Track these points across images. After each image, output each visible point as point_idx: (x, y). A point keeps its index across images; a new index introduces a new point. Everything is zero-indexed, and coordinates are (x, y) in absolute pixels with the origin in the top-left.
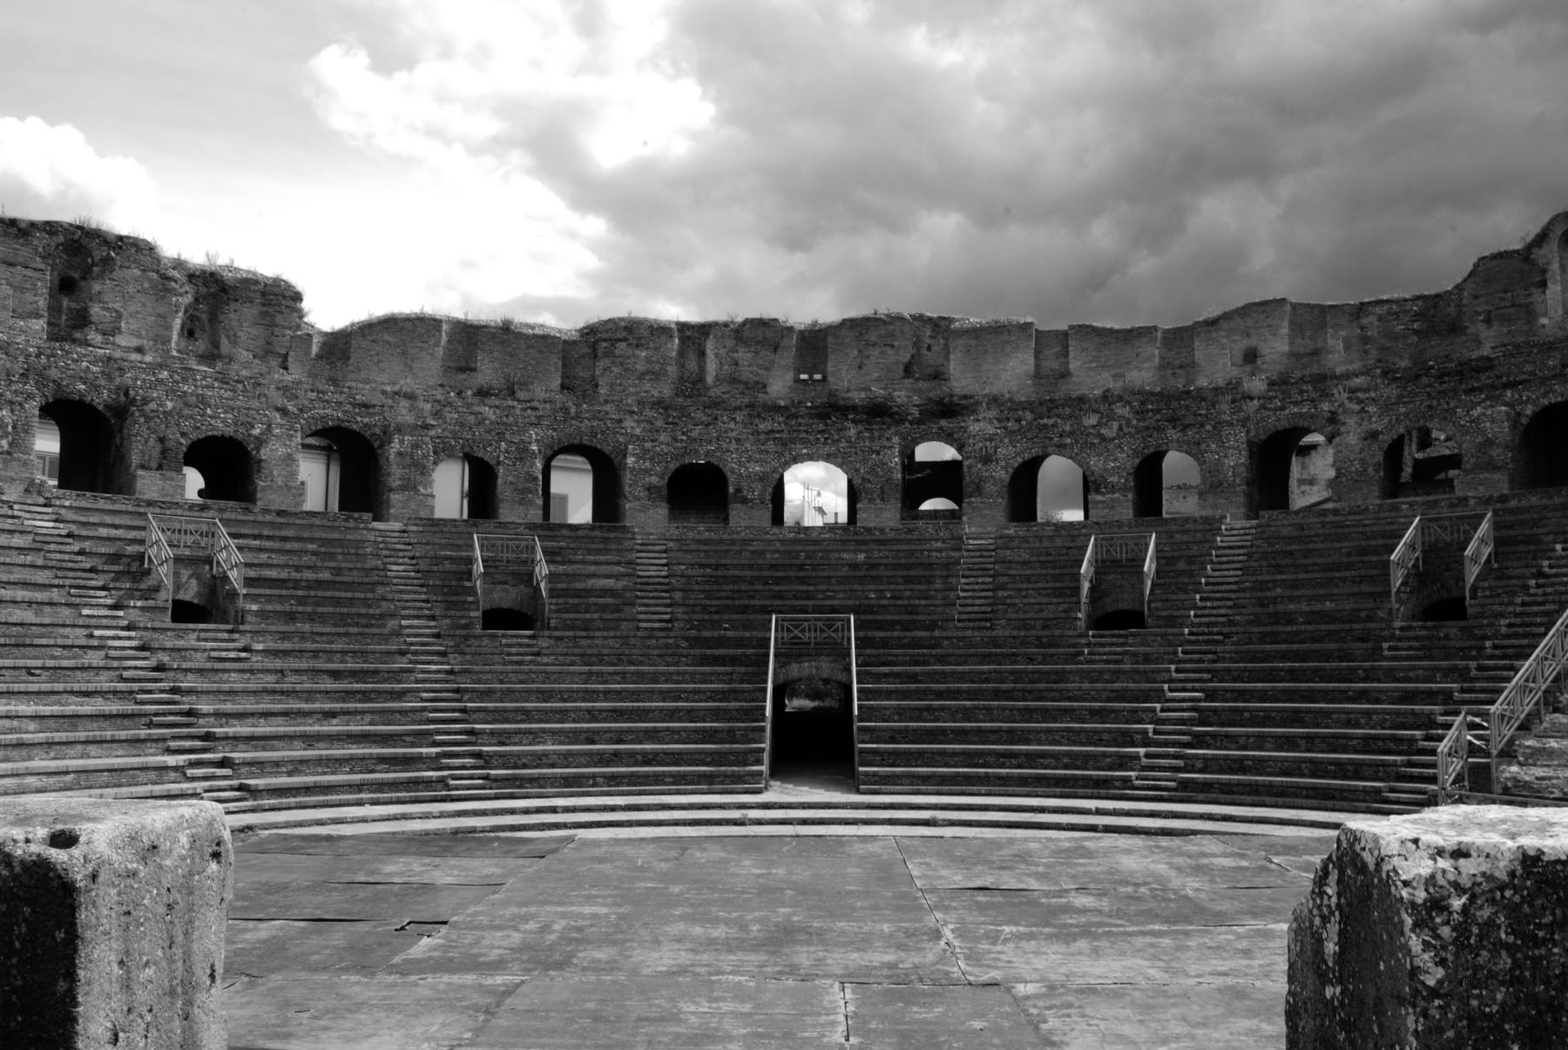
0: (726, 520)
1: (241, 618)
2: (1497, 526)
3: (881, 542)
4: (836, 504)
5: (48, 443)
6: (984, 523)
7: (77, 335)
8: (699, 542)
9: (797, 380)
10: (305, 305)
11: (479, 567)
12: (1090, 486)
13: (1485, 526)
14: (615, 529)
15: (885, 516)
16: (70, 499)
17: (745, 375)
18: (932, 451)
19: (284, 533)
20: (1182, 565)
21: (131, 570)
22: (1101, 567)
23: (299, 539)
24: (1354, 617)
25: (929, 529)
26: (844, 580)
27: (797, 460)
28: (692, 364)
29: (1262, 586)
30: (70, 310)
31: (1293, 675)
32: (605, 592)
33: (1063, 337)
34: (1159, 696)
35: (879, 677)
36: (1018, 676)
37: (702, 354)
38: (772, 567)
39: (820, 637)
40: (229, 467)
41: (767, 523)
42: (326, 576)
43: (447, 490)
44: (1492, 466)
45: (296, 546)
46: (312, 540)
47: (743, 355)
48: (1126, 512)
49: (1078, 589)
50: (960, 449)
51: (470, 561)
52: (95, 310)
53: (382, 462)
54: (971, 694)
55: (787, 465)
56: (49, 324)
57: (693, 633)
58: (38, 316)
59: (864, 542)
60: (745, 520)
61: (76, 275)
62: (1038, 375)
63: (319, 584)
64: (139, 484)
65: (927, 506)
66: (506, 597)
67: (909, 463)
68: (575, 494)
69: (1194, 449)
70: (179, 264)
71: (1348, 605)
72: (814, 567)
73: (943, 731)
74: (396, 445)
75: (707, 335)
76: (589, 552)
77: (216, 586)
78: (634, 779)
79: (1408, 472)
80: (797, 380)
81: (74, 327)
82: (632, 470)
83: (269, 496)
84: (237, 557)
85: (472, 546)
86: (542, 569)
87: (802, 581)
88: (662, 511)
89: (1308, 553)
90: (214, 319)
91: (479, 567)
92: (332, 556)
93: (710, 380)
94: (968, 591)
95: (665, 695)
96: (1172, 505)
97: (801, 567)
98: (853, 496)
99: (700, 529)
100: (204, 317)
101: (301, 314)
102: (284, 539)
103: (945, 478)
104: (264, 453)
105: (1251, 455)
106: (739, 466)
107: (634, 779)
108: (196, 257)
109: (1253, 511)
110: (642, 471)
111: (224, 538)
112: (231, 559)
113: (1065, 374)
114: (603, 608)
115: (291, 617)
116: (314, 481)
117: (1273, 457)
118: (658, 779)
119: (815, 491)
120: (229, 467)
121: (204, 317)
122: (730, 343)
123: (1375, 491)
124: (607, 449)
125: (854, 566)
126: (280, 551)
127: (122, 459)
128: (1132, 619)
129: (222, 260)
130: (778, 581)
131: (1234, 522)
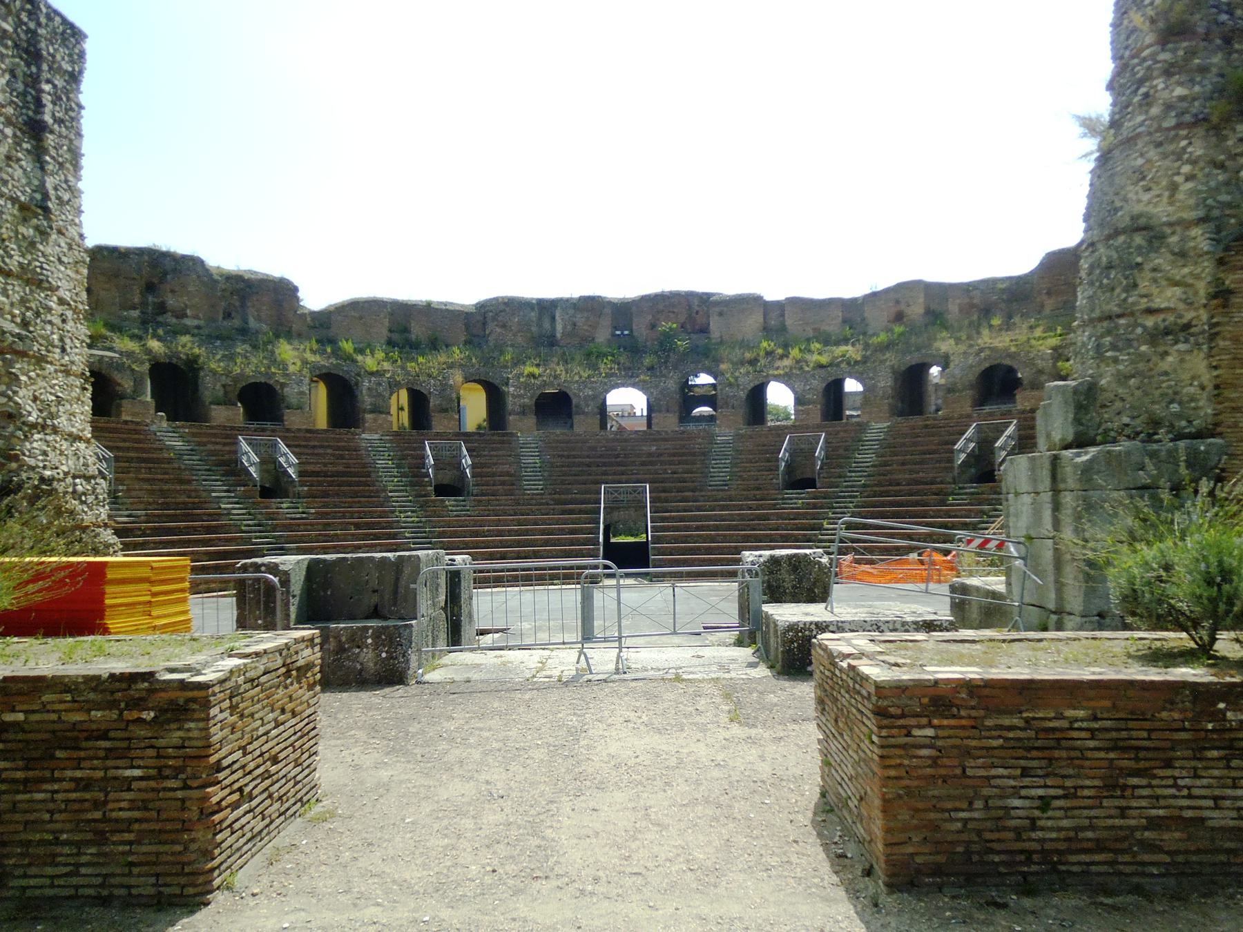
0: (572, 426)
2: (1019, 428)
3: (665, 440)
7: (160, 319)
8: (558, 441)
9: (614, 335)
10: (300, 294)
13: (1011, 429)
14: (504, 435)
15: (669, 422)
19: (312, 443)
20: (841, 451)
22: (793, 452)
23: (321, 447)
30: (154, 303)
34: (820, 528)
35: (663, 519)
36: (742, 518)
37: (553, 318)
38: (601, 456)
39: (630, 497)
41: (597, 428)
42: (341, 468)
45: (321, 451)
46: (328, 447)
49: (777, 468)
50: (715, 378)
51: (423, 457)
53: (357, 393)
54: (717, 528)
55: (607, 391)
56: (142, 312)
57: (557, 496)
58: (135, 308)
59: (655, 440)
60: (583, 426)
61: (155, 281)
63: (338, 474)
64: (213, 414)
66: (447, 477)
67: (685, 386)
72: (626, 456)
73: (699, 548)
75: (556, 307)
76: (493, 449)
80: (614, 335)
81: (158, 314)
82: (514, 396)
83: (293, 420)
85: (424, 449)
86: (467, 461)
87: (619, 464)
88: (531, 420)
89: (915, 444)
92: (342, 457)
93: (559, 335)
94: (720, 471)
95: (543, 532)
97: (618, 456)
99: (558, 432)
100: (237, 304)
101: (298, 299)
102: (314, 447)
105: (896, 380)
114: (503, 483)
115: (326, 494)
119: (628, 400)
121: (237, 304)
122: (571, 312)
123: (969, 402)
124: (496, 382)
125: (650, 455)
126: (313, 454)
128: (810, 483)
129: (243, 268)
130: (605, 464)
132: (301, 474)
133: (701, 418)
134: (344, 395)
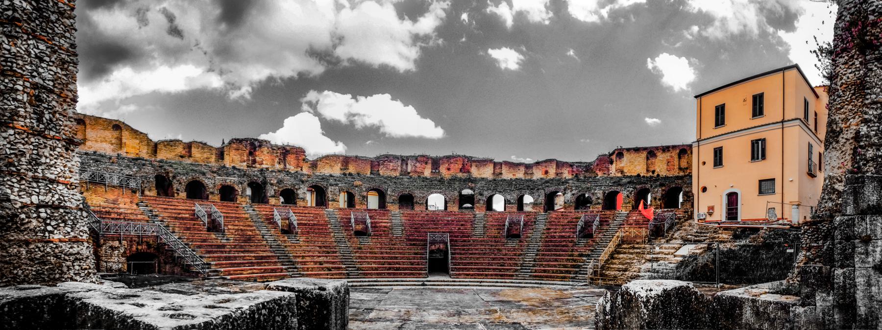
1: (297, 233)
4: (441, 207)
5: (249, 192)
6: (480, 212)
11: (353, 220)
12: (507, 202)
15: (454, 208)
16: (256, 206)
17: (418, 170)
18: (467, 192)
21: (270, 221)
24: (569, 237)
25: (467, 212)
26: (445, 225)
27: (432, 193)
28: (404, 167)
29: (549, 229)
31: (556, 250)
32: (385, 227)
33: (501, 164)
40: (290, 196)
43: (342, 199)
44: (599, 203)
47: (418, 165)
48: (515, 210)
51: (350, 219)
52: (257, 159)
60: (418, 209)
62: (494, 173)
65: (465, 205)
66: (360, 227)
67: (461, 195)
68: (373, 202)
69: (531, 194)
70: (276, 146)
71: (568, 234)
74: (330, 189)
77: (291, 225)
78: (394, 274)
79: (581, 202)
84: (296, 218)
86: (369, 221)
88: (397, 206)
90: (285, 159)
91: (353, 220)
96: (527, 209)
98: (446, 202)
103: (470, 199)
104: (299, 192)
106: (417, 194)
107: (394, 274)
108: (280, 143)
109: (545, 211)
110: (392, 194)
111: (291, 213)
112: (294, 219)
113: (501, 174)
116: (310, 199)
117: (550, 200)
118: (400, 274)
119: (436, 201)
120: (290, 196)
127: (265, 196)
128: (518, 236)
131: (542, 215)
132: (298, 224)
133: (468, 208)
134: (321, 194)
